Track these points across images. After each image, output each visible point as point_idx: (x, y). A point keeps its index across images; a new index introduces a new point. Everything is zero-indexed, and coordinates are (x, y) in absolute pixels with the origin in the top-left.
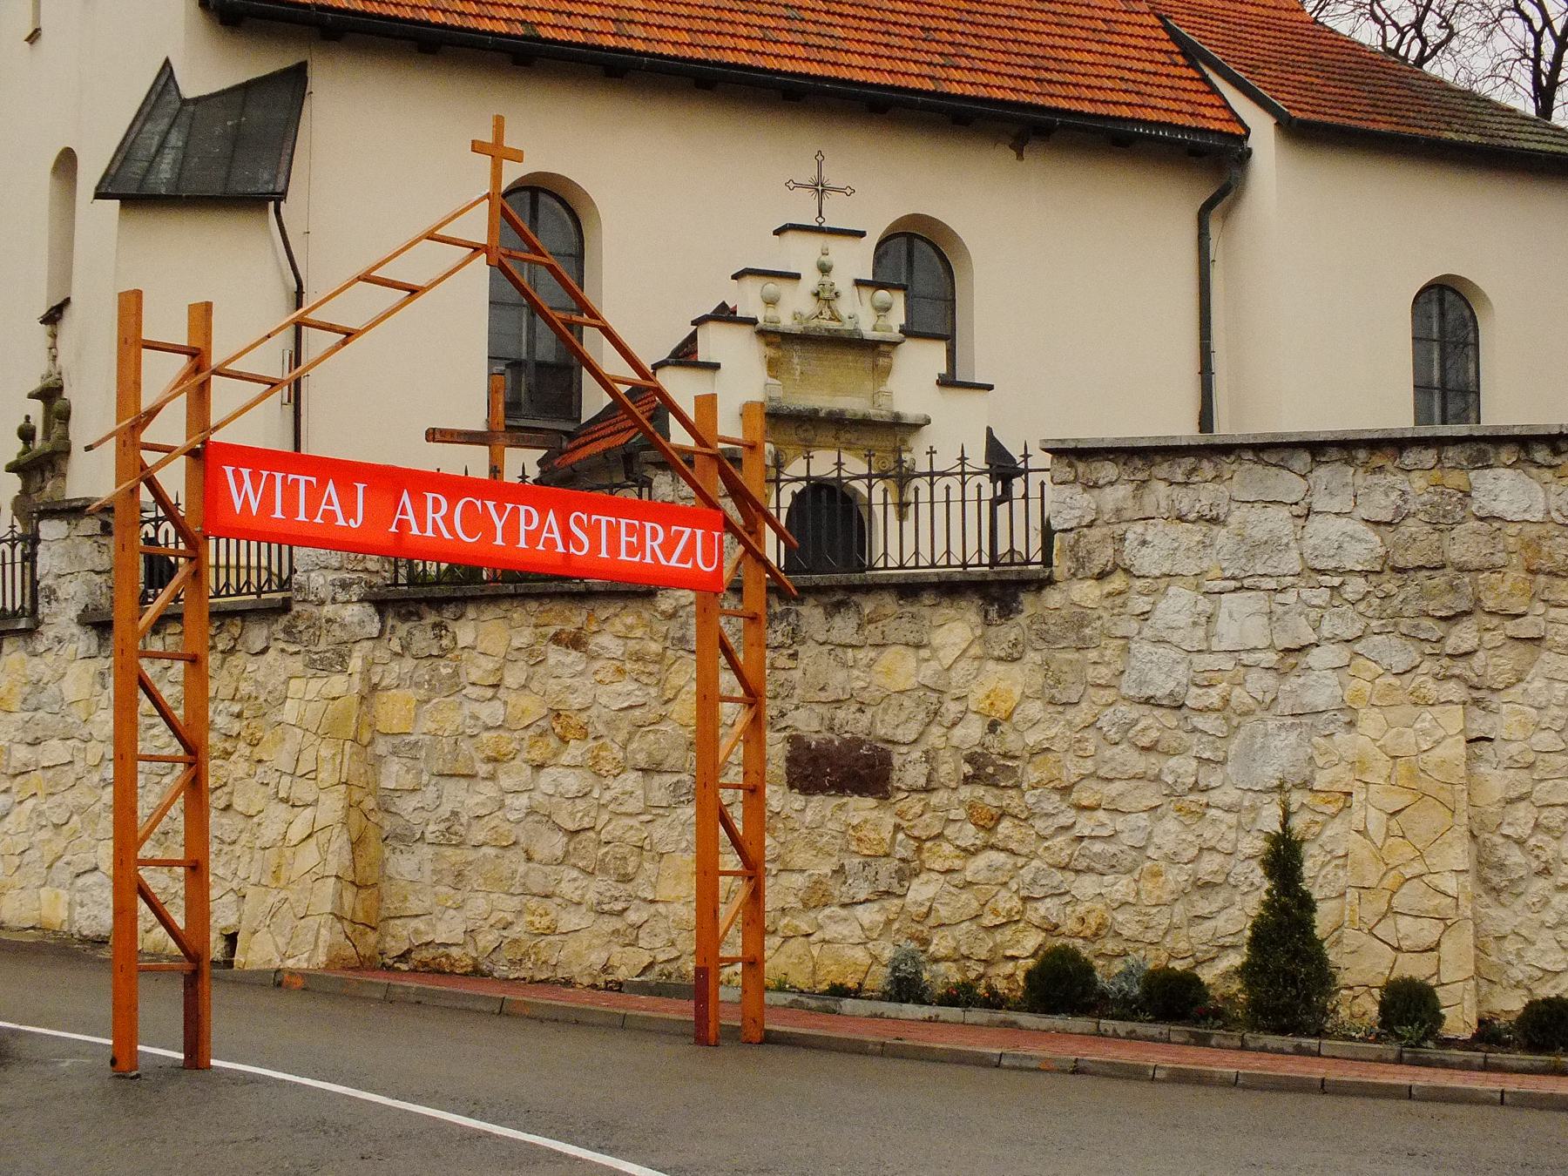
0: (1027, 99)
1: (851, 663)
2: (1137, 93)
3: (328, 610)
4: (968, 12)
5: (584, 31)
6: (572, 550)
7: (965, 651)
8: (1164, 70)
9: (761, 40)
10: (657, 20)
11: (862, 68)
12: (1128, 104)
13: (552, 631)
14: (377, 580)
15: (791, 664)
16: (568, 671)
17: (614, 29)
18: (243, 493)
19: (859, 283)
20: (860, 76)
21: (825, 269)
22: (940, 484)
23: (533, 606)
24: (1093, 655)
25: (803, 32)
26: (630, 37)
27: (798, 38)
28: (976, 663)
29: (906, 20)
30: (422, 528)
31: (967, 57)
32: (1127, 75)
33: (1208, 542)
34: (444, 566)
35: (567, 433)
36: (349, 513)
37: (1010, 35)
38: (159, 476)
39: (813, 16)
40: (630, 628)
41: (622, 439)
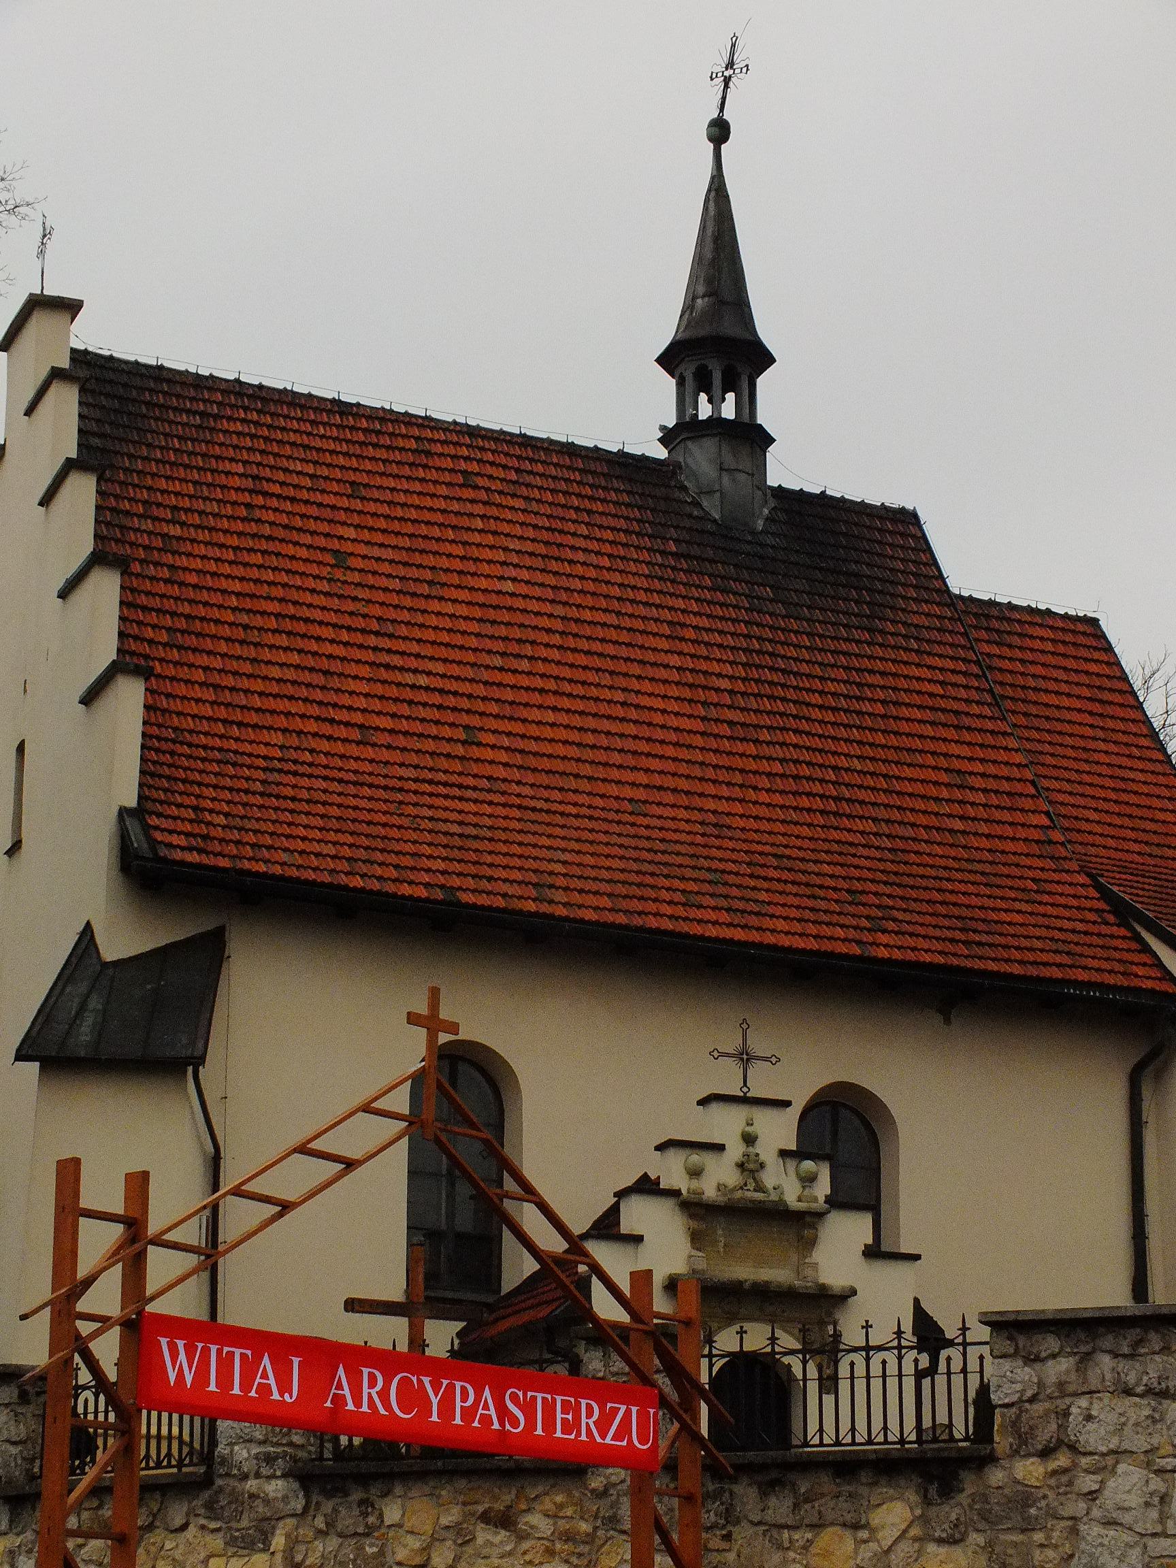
0: (955, 961)
1: (786, 1544)
2: (1068, 953)
3: (251, 1485)
4: (896, 874)
5: (505, 895)
6: (508, 1427)
7: (905, 1531)
8: (1095, 929)
9: (684, 905)
10: (579, 884)
11: (787, 933)
12: (1059, 965)
13: (480, 1509)
14: (301, 1454)
15: (724, 1545)
16: (496, 1551)
17: (534, 893)
18: (178, 1366)
19: (784, 1154)
20: (786, 941)
21: (749, 1139)
22: (877, 1358)
23: (462, 1483)
24: (1039, 1537)
25: (726, 897)
26: (551, 902)
27: (723, 903)
28: (917, 1545)
29: (831, 883)
30: (358, 1403)
31: (895, 920)
32: (1057, 935)
33: (1157, 1416)
34: (357, 1441)
35: (487, 1305)
36: (284, 1387)
37: (944, 874)
38: (94, 1347)
39: (738, 880)
40: (560, 1507)
41: (544, 1312)
